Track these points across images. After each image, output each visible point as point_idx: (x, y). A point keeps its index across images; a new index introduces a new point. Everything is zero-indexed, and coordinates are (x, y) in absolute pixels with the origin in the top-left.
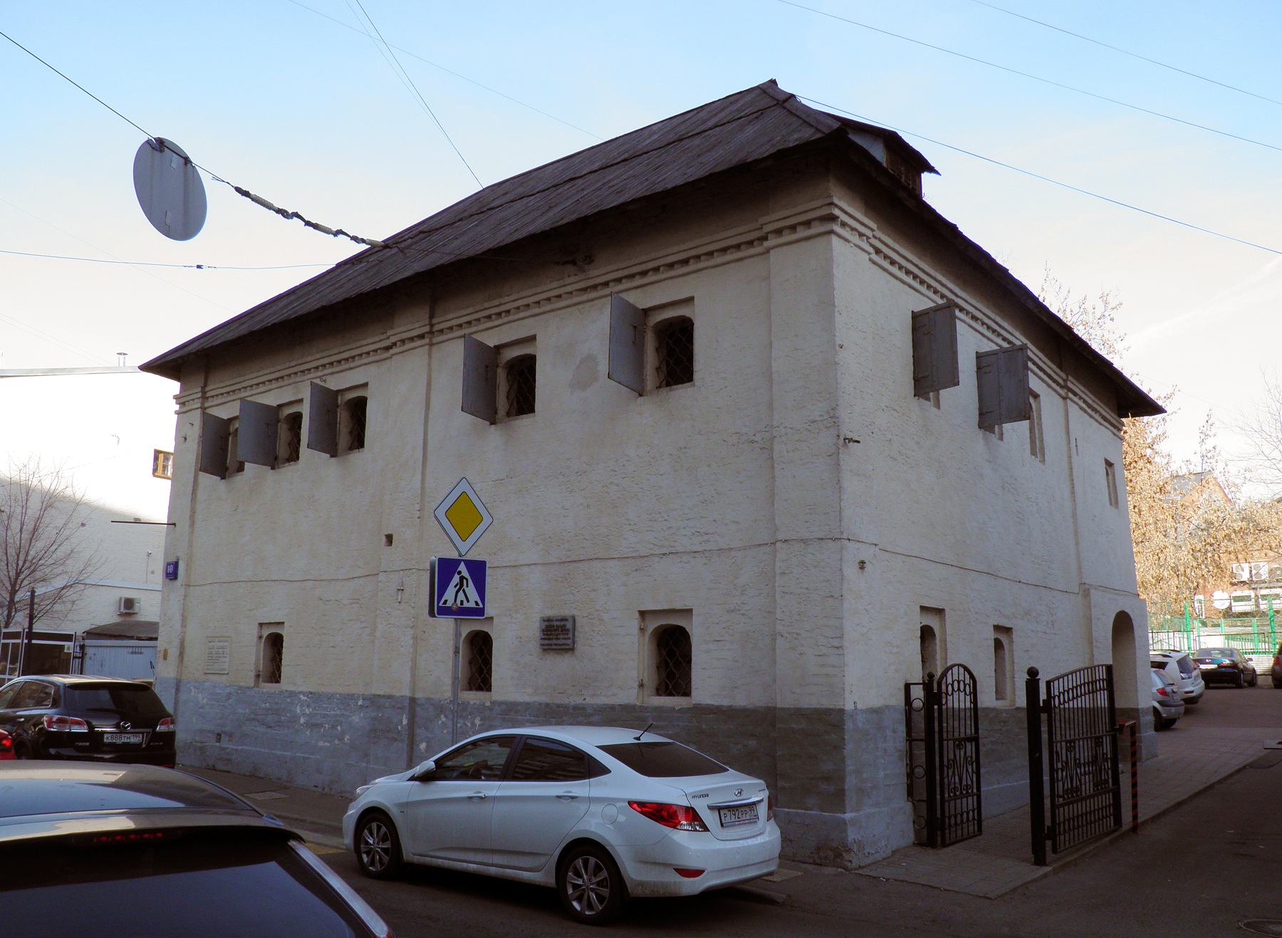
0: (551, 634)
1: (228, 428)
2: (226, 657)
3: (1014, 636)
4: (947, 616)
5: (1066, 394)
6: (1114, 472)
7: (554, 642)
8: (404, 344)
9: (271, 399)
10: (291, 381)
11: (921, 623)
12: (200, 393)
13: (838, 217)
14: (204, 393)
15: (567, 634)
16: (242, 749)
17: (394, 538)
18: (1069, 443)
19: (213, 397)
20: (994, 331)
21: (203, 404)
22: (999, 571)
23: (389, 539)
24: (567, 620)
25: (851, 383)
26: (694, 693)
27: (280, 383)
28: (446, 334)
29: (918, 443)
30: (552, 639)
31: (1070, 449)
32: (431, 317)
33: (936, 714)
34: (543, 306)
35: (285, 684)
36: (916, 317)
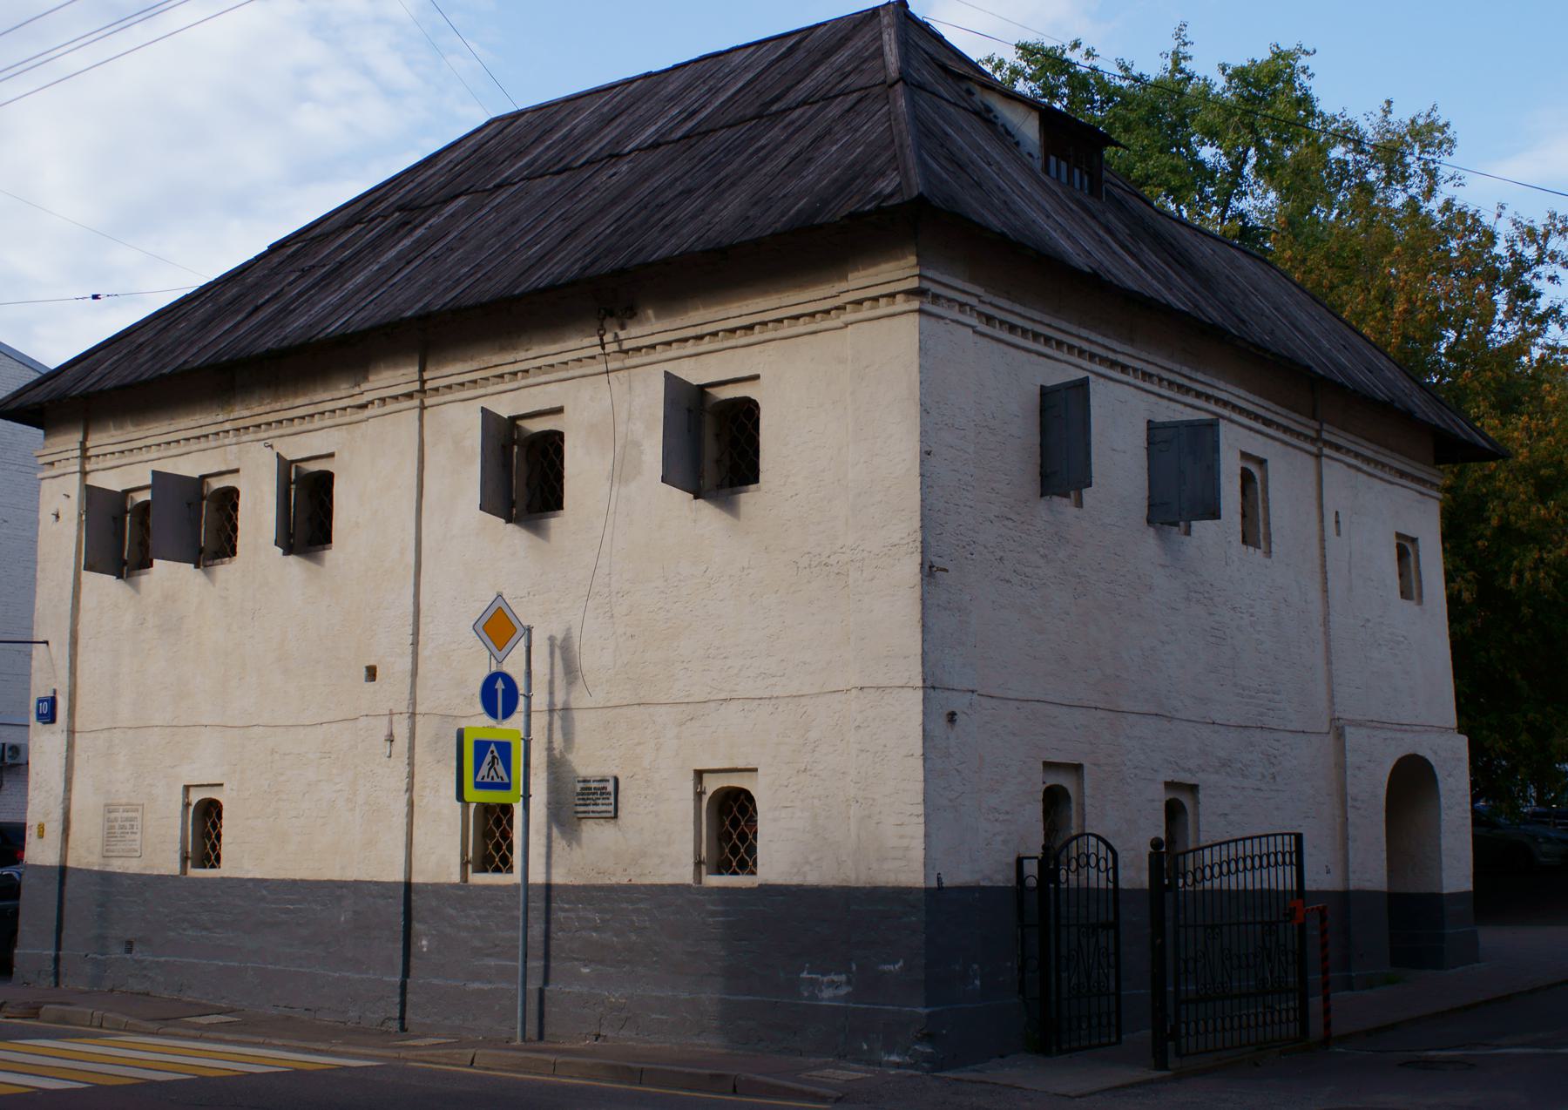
0: (588, 799)
1: (125, 503)
2: (136, 833)
3: (1200, 796)
4: (1085, 772)
5: (1319, 448)
6: (1418, 550)
7: (591, 808)
8: (384, 404)
9: (189, 467)
10: (219, 443)
11: (1044, 783)
12: (79, 451)
13: (929, 290)
14: (84, 449)
15: (608, 799)
16: (166, 961)
17: (378, 669)
18: (1322, 520)
19: (98, 456)
20: (1180, 387)
21: (82, 466)
22: (1177, 711)
23: (371, 673)
24: (608, 781)
25: (942, 497)
26: (760, 869)
27: (203, 444)
28: (443, 395)
29: (1044, 556)
30: (589, 805)
31: (1322, 529)
32: (422, 369)
33: (1052, 896)
34: (572, 369)
35: (226, 869)
36: (1045, 392)
